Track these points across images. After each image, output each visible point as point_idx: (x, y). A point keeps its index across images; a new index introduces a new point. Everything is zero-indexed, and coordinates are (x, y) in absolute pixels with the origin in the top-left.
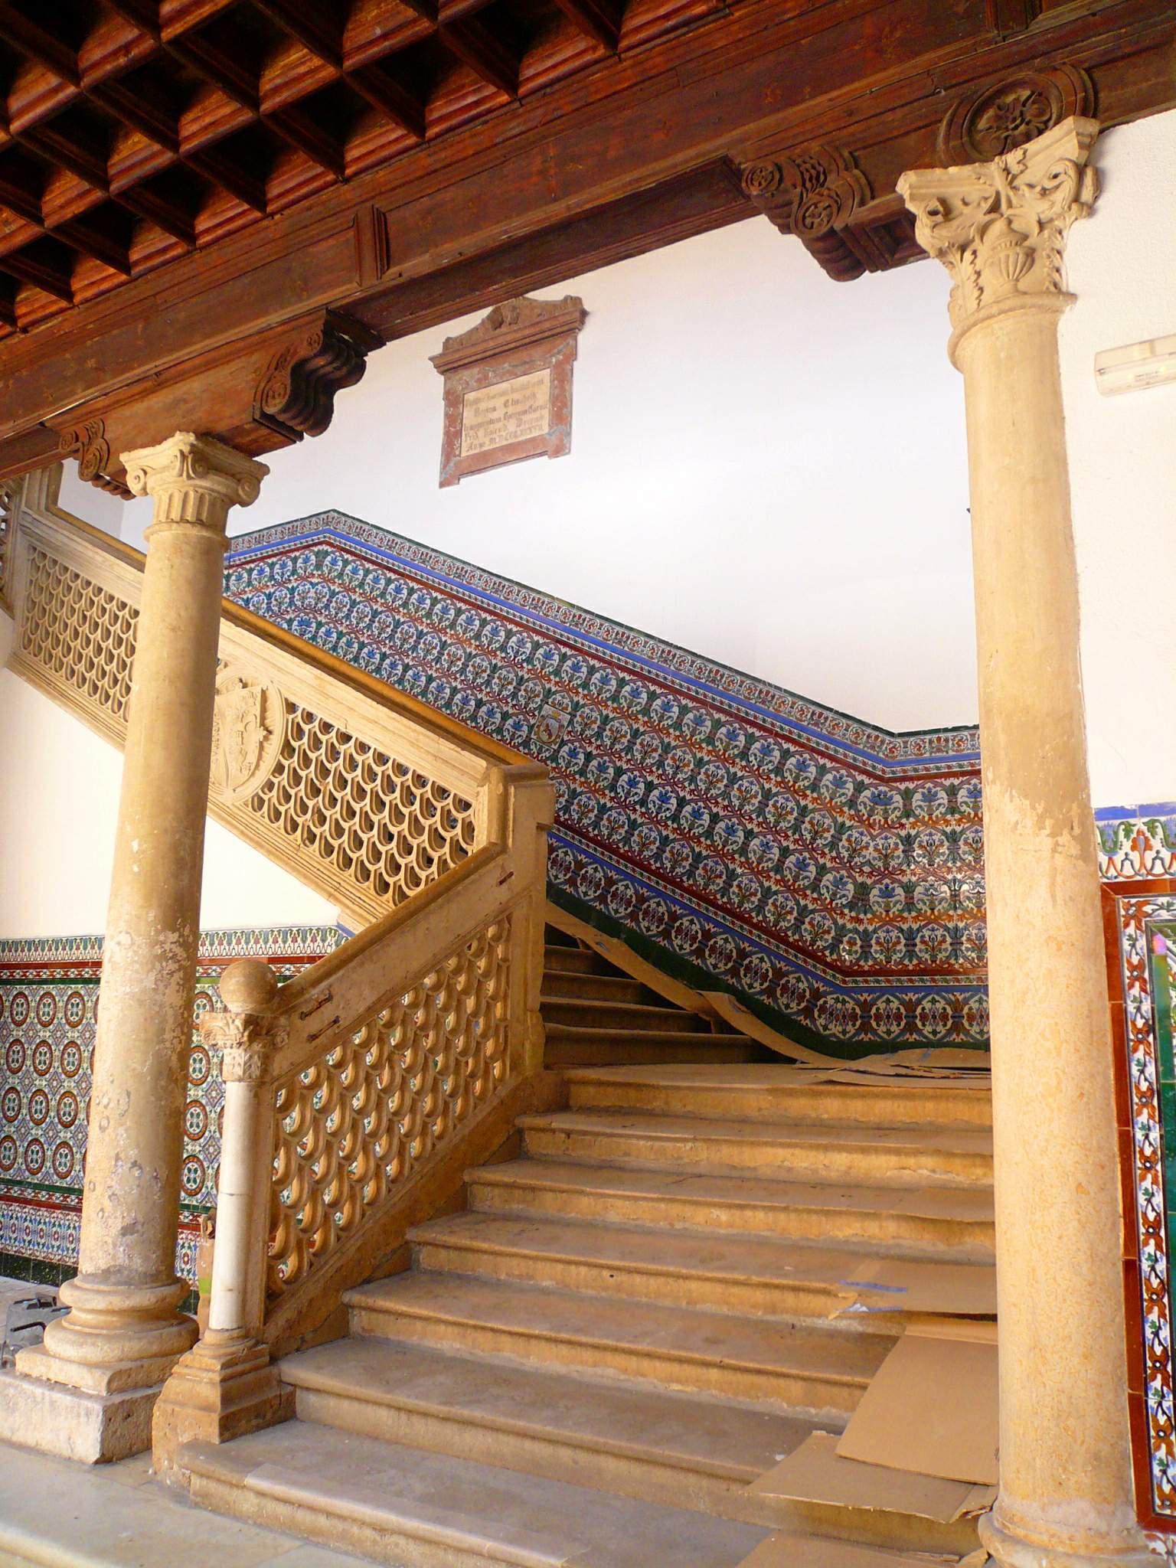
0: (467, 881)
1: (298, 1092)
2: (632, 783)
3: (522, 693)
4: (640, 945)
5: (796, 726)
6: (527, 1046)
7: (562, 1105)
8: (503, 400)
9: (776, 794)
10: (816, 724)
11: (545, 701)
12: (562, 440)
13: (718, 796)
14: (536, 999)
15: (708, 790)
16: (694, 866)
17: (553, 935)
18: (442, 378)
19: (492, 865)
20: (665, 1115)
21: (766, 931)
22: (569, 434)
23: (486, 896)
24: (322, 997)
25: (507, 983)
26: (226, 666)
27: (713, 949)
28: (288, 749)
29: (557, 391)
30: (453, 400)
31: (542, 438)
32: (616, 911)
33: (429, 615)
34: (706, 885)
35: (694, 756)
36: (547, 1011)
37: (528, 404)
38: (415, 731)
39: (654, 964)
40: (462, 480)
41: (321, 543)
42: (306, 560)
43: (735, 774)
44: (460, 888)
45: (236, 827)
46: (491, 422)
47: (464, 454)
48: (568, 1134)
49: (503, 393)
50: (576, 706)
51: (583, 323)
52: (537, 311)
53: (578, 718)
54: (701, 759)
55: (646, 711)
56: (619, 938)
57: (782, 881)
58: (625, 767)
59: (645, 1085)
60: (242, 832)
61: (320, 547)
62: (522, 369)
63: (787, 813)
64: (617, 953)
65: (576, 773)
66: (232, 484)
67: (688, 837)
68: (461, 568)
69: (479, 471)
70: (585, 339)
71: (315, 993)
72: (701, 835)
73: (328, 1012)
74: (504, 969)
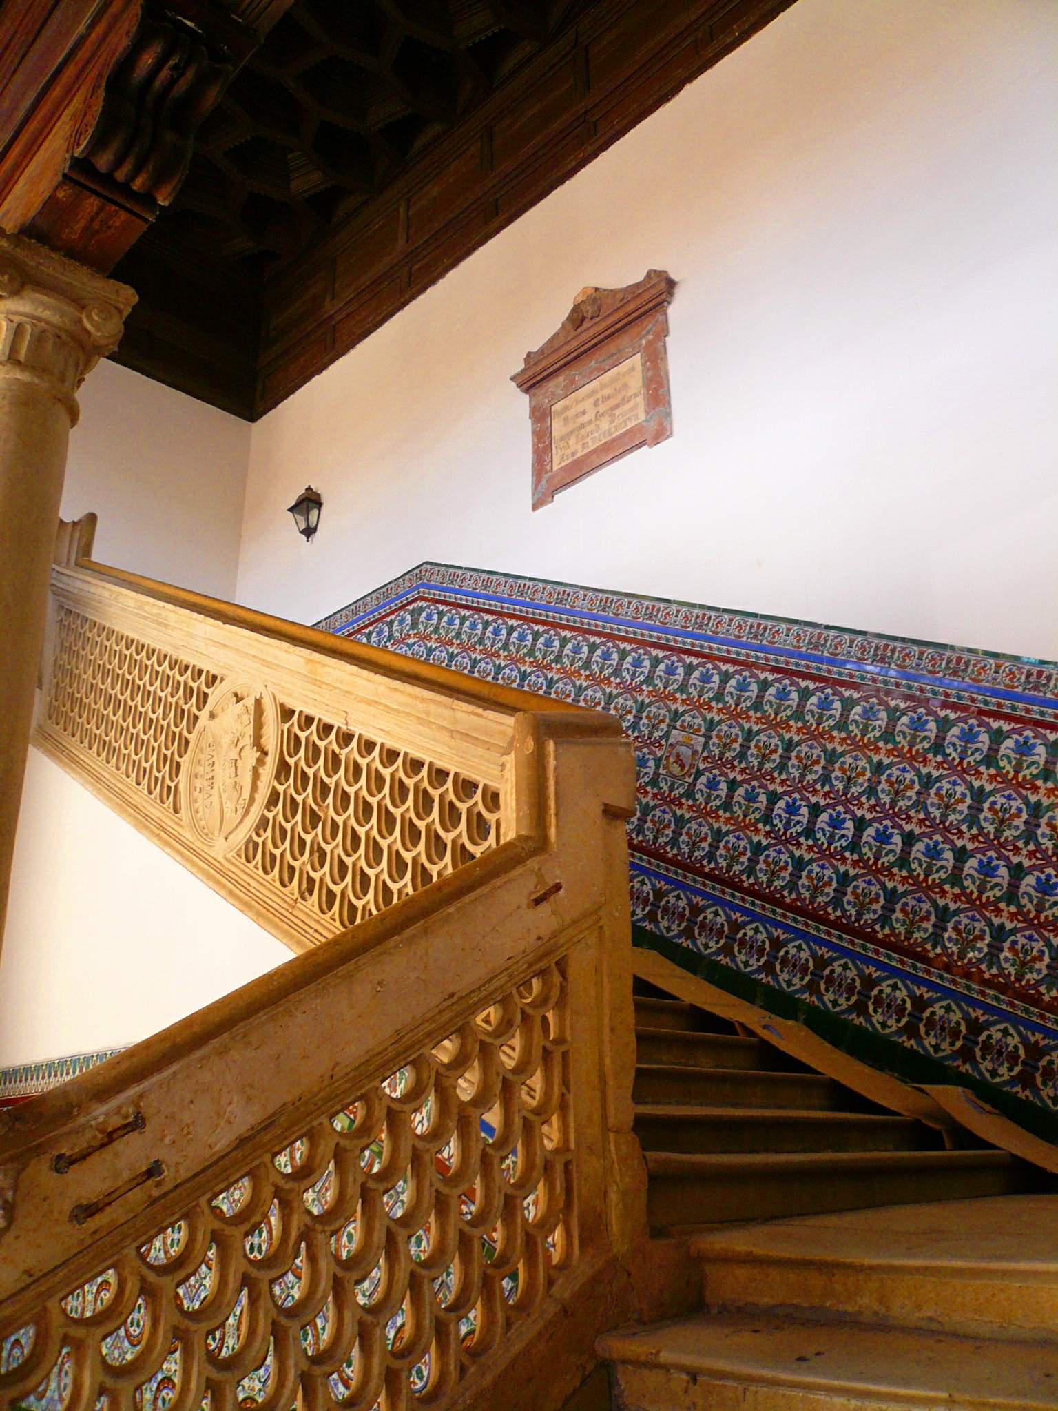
0: (466, 899)
1: (57, 1333)
2: (792, 809)
3: (645, 721)
4: (826, 1026)
5: (1007, 695)
6: (613, 1197)
7: (690, 1303)
8: (591, 400)
9: (992, 793)
10: (1036, 688)
11: (671, 727)
12: (661, 424)
13: (909, 808)
14: (623, 1110)
15: (893, 803)
16: (889, 909)
17: (642, 987)
18: (526, 398)
19: (519, 870)
20: (882, 1326)
21: (1003, 989)
22: (669, 414)
23: (509, 925)
24: (117, 1121)
25: (565, 1083)
26: (222, 679)
27: (930, 1024)
28: (283, 769)
29: (650, 374)
30: (540, 416)
31: (638, 429)
32: (789, 983)
33: (531, 652)
34: (909, 934)
35: (870, 760)
36: (649, 1131)
37: (620, 397)
38: (423, 700)
39: (851, 1052)
40: (556, 497)
41: (415, 600)
42: (402, 622)
43: (929, 775)
44: (451, 909)
45: (224, 886)
46: (582, 426)
47: (555, 468)
48: (694, 1376)
49: (594, 392)
50: (711, 725)
51: (671, 294)
52: (620, 296)
53: (715, 740)
54: (880, 763)
55: (799, 714)
56: (796, 1020)
57: (1020, 914)
58: (780, 790)
59: (837, 1265)
60: (231, 893)
61: (415, 605)
62: (610, 361)
63: (1012, 817)
64: (793, 1039)
65: (718, 808)
66: (71, 310)
67: (876, 871)
68: (561, 591)
69: (574, 481)
70: (675, 311)
71: (102, 1113)
72: (892, 865)
73: (132, 1153)
74: (557, 1058)
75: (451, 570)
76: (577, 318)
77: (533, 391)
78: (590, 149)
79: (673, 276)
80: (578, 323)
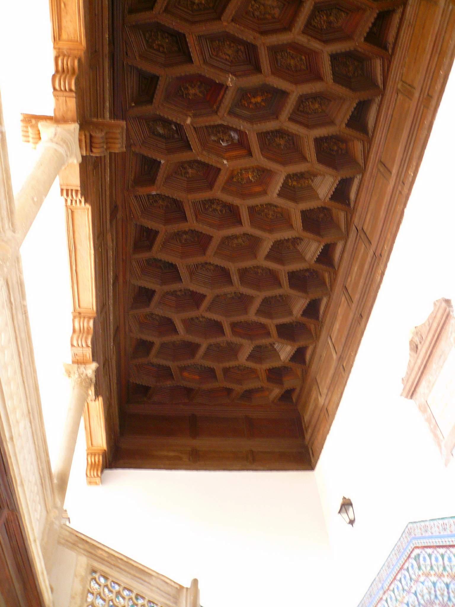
30: (424, 408)
52: (427, 324)
75: (423, 524)
76: (415, 348)
77: (414, 397)
78: (382, 267)
79: (447, 298)
80: (415, 349)
